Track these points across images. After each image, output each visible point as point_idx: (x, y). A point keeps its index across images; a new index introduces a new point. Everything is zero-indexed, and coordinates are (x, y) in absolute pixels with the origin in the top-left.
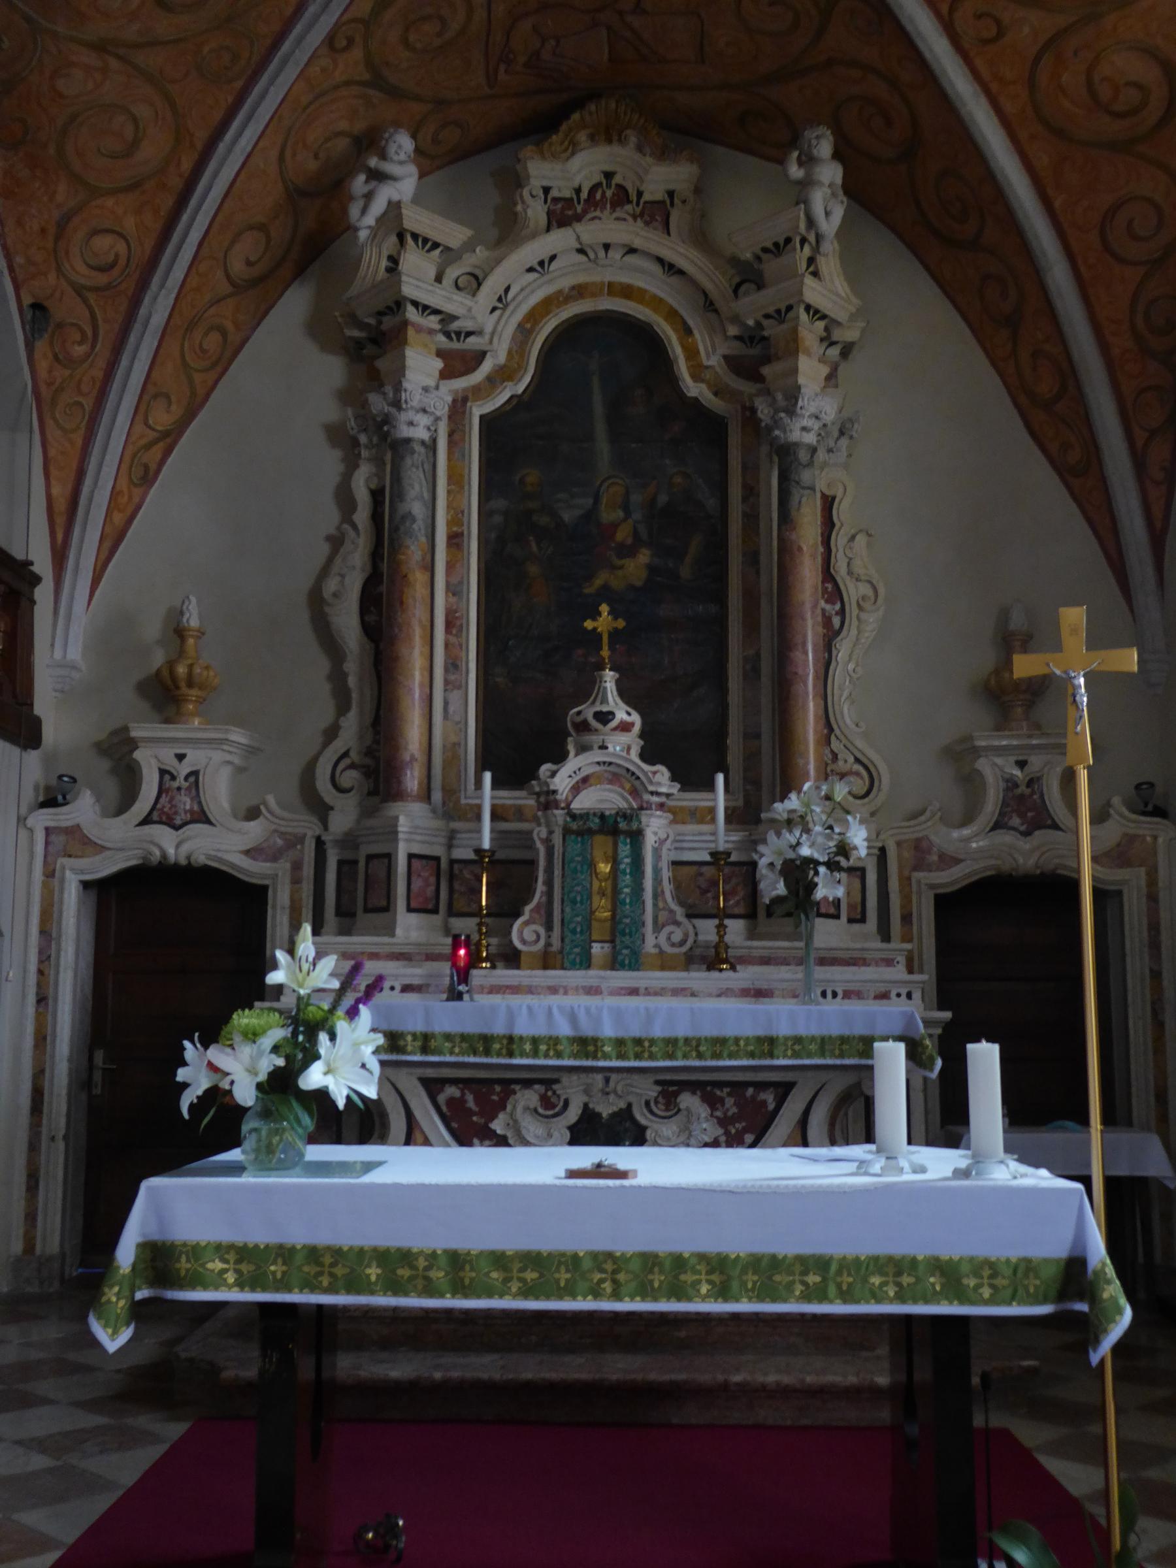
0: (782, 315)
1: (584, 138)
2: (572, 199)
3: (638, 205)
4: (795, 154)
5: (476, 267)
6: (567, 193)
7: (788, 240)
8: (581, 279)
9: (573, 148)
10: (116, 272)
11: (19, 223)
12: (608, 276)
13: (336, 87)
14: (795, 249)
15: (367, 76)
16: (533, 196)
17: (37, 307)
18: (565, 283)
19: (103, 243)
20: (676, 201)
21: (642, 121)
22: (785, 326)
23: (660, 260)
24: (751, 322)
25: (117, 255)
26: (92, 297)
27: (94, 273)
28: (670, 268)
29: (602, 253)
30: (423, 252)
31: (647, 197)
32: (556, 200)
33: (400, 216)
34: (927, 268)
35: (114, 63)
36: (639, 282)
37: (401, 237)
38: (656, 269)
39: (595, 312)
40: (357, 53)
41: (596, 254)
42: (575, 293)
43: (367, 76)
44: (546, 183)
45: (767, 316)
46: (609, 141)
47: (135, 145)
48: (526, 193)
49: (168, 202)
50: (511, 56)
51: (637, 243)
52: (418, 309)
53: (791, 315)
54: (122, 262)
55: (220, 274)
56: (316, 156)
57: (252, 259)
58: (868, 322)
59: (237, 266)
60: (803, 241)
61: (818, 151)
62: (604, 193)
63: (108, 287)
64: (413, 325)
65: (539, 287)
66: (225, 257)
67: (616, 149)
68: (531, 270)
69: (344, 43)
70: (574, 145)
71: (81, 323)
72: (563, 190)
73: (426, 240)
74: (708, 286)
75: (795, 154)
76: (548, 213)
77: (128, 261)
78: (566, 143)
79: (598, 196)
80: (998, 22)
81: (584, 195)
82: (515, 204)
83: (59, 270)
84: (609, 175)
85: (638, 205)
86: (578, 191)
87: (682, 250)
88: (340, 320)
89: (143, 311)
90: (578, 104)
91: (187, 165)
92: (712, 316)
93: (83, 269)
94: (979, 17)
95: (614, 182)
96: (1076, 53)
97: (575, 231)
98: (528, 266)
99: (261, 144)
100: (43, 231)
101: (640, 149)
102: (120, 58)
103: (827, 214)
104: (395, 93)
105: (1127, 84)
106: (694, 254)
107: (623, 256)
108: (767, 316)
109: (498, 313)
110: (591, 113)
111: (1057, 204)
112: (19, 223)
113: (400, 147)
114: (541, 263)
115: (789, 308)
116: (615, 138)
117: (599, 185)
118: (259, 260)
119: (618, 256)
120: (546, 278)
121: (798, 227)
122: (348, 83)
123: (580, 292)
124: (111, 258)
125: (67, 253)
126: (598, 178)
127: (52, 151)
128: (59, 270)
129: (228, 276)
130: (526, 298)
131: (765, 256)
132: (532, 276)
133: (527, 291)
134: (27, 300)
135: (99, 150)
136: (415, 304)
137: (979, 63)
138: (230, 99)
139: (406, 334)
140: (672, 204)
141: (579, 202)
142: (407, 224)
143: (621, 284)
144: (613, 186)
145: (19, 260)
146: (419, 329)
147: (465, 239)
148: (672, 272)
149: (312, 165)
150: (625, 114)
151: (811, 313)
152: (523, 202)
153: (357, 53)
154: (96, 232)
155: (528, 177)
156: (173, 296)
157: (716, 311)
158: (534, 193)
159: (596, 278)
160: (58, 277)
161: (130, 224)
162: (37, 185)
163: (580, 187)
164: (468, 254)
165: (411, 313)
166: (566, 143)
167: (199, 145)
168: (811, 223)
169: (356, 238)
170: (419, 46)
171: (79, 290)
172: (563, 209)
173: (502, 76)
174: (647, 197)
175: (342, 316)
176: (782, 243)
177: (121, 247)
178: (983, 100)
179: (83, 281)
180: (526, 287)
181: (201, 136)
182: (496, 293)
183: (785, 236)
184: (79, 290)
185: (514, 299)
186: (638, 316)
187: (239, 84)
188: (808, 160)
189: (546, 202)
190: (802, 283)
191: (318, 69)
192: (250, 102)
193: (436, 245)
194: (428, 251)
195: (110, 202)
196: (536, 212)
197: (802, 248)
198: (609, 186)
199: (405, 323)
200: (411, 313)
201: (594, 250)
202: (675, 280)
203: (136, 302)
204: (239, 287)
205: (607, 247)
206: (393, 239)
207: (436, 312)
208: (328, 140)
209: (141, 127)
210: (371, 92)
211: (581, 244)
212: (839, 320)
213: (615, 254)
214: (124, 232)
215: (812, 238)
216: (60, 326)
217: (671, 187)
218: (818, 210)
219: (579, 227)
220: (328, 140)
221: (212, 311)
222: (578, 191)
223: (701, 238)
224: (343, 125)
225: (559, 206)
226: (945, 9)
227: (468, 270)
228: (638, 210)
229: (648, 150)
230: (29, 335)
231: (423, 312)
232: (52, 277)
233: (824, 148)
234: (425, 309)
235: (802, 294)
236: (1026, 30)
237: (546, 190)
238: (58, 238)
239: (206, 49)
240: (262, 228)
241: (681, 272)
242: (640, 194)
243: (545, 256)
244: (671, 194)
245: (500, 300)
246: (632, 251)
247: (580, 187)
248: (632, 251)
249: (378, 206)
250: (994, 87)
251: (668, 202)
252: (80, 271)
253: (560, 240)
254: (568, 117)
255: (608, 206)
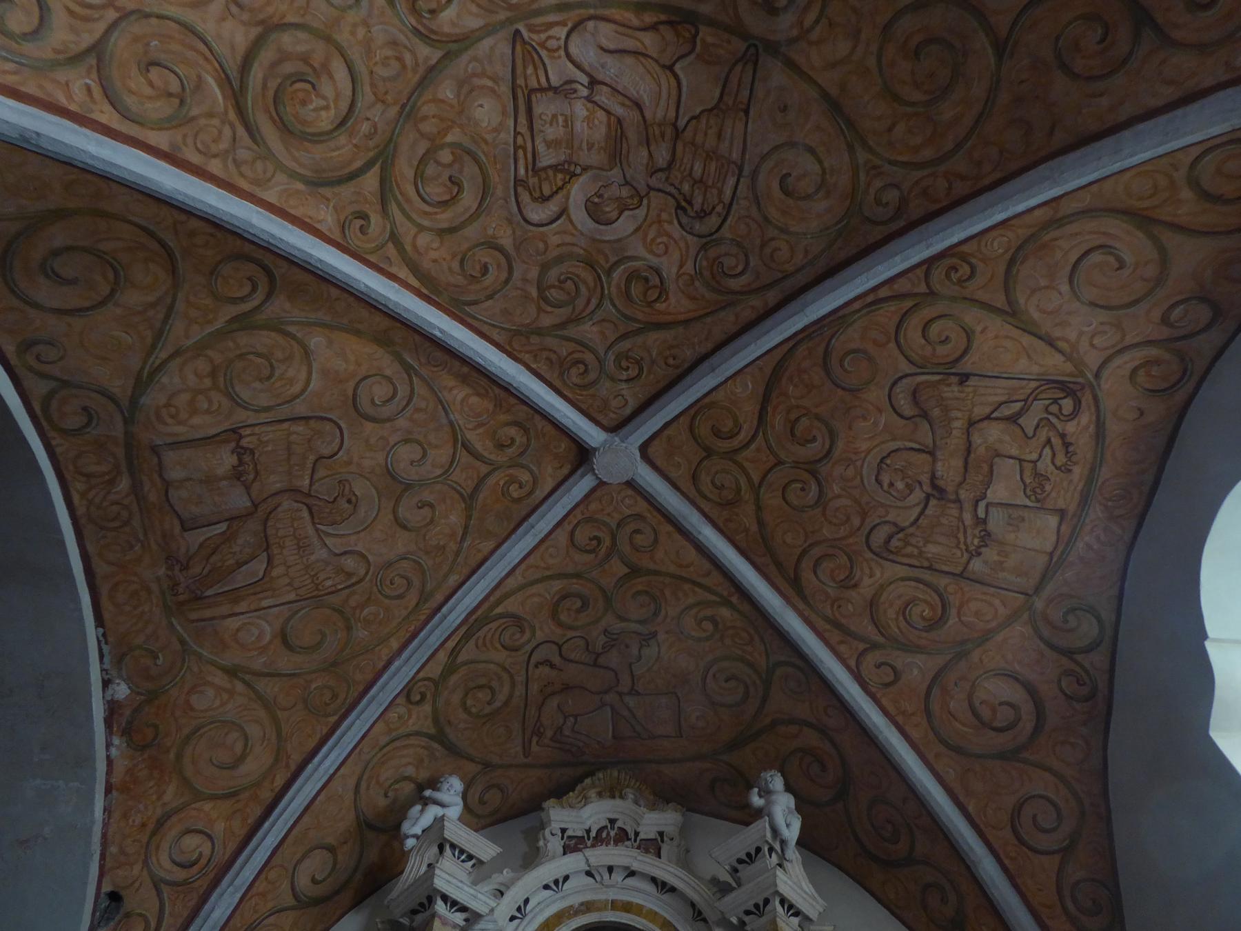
0: (758, 909)
1: (594, 795)
2: (583, 837)
3: (635, 841)
4: (756, 790)
5: (501, 884)
6: (579, 833)
7: (758, 850)
8: (589, 897)
9: (586, 800)
10: (195, 869)
11: (125, 816)
12: (612, 895)
13: (408, 735)
14: (765, 855)
15: (433, 731)
16: (553, 835)
17: (115, 897)
18: (575, 900)
19: (191, 842)
20: (665, 839)
21: (638, 784)
22: (764, 920)
23: (654, 880)
24: (734, 920)
25: (201, 854)
26: (166, 890)
27: (176, 868)
28: (663, 887)
29: (606, 876)
30: (459, 861)
31: (642, 836)
32: (570, 837)
33: (442, 828)
34: (873, 894)
35: (240, 687)
36: (637, 899)
37: (441, 848)
38: (651, 888)
39: (599, 922)
40: (427, 708)
41: (602, 877)
42: (583, 908)
43: (433, 731)
44: (563, 826)
45: (748, 913)
46: (613, 797)
47: (241, 759)
48: (547, 832)
49: (258, 811)
50: (542, 730)
51: (635, 866)
52: (446, 904)
53: (768, 908)
54: (203, 861)
55: (285, 885)
56: (386, 796)
57: (318, 877)
58: (835, 926)
59: (303, 881)
60: (771, 850)
61: (773, 785)
62: (608, 834)
63: (185, 883)
64: (440, 917)
65: (554, 902)
66: (295, 869)
67: (618, 802)
68: (546, 887)
69: (418, 697)
70: (586, 798)
71: (148, 915)
72: (576, 830)
73: (462, 851)
74: (695, 897)
75: (756, 790)
76: (564, 847)
77: (209, 860)
78: (580, 798)
79: (604, 835)
80: (893, 668)
81: (593, 834)
82: (538, 841)
83: (146, 862)
84: (612, 821)
85: (635, 841)
86: (588, 831)
87: (672, 870)
88: (380, 926)
89: (207, 907)
90: (591, 774)
91: (279, 782)
92: (701, 924)
93: (167, 864)
94: (878, 666)
95: (616, 826)
96: (956, 684)
97: (585, 856)
98: (544, 883)
99: (342, 771)
100: (144, 825)
101: (636, 802)
102: (248, 684)
103: (788, 826)
104: (453, 750)
105: (1001, 704)
106: (681, 873)
107: (627, 877)
108: (748, 913)
109: (517, 921)
110: (599, 780)
111: (971, 809)
112: (125, 816)
113: (451, 786)
114: (556, 882)
115: (767, 901)
116: (617, 794)
117: (605, 827)
118: (324, 880)
119: (620, 879)
120: (561, 894)
121: (765, 836)
122: (417, 734)
123: (588, 907)
124: (196, 856)
125: (158, 848)
126: (604, 823)
127: (172, 756)
128: (146, 862)
129: (293, 889)
130: (541, 910)
131: (740, 867)
132: (548, 893)
133: (542, 906)
134: (107, 888)
135: (211, 760)
136: (445, 898)
137: (884, 702)
138: (325, 731)
139: (433, 924)
140: (662, 841)
141: (589, 839)
142: (447, 835)
143: (622, 901)
144: (616, 829)
145: (113, 849)
146: (445, 922)
147: (495, 855)
148: (665, 890)
149: (382, 802)
150: (625, 780)
151: (786, 907)
152: (545, 839)
153: (427, 708)
154: (189, 831)
155: (550, 821)
156: (239, 895)
157: (705, 920)
158: (553, 832)
159: (602, 897)
160: (143, 868)
161: (219, 828)
162: (151, 784)
163: (590, 828)
164: (497, 875)
165: (440, 907)
166: (580, 798)
167: (293, 767)
168: (775, 832)
169: (402, 844)
170: (474, 710)
171: (157, 884)
172: (576, 844)
173: (535, 748)
174: (642, 836)
175: (383, 922)
176: (753, 853)
177: (206, 849)
178: (893, 729)
179: (162, 874)
180: (542, 902)
181: (296, 758)
182: (516, 902)
183: (755, 846)
184: (157, 884)
185: (531, 911)
186: (638, 926)
187: (333, 719)
188: (766, 793)
189: (562, 839)
190: (775, 876)
191: (396, 715)
192: (338, 733)
193: (470, 857)
194: (463, 861)
195: (207, 806)
196: (555, 844)
197: (771, 857)
198: (612, 828)
199: (434, 915)
200: (440, 907)
201: (600, 874)
202: (666, 897)
203: (204, 899)
204: (303, 903)
205: (610, 869)
206: (435, 850)
207: (463, 909)
208: (397, 782)
209: (250, 745)
210: (436, 745)
211: (589, 866)
212: (811, 917)
213: (618, 877)
214: (213, 835)
215: (777, 847)
216: (128, 915)
217: (661, 829)
218: (780, 819)
219: (588, 852)
220: (397, 782)
221: (272, 920)
222: (588, 831)
223: (685, 861)
224: (410, 771)
225: (573, 842)
226: (852, 663)
227: (497, 887)
228: (636, 845)
229: (642, 802)
230: (96, 923)
231: (451, 907)
232: (137, 869)
233: (777, 783)
234: (454, 904)
235: (776, 885)
236: (916, 672)
237: (563, 831)
238: (154, 833)
239: (313, 686)
240: (331, 849)
241: (673, 890)
242: (637, 834)
243: (560, 876)
244: (661, 834)
245: (519, 909)
246: (632, 874)
247: (590, 828)
248: (632, 874)
249: (427, 819)
250: (900, 719)
251: (659, 839)
252: (164, 864)
253: (574, 862)
254: (582, 782)
255: (612, 842)
